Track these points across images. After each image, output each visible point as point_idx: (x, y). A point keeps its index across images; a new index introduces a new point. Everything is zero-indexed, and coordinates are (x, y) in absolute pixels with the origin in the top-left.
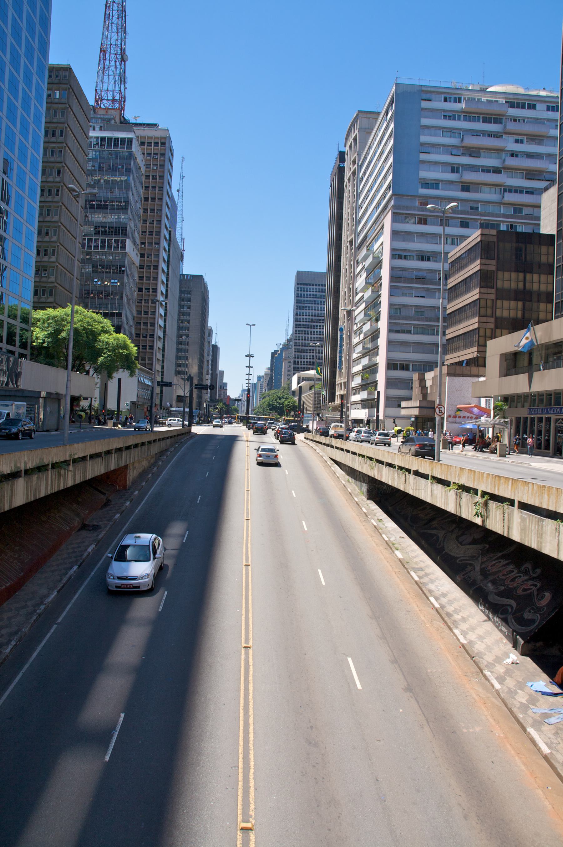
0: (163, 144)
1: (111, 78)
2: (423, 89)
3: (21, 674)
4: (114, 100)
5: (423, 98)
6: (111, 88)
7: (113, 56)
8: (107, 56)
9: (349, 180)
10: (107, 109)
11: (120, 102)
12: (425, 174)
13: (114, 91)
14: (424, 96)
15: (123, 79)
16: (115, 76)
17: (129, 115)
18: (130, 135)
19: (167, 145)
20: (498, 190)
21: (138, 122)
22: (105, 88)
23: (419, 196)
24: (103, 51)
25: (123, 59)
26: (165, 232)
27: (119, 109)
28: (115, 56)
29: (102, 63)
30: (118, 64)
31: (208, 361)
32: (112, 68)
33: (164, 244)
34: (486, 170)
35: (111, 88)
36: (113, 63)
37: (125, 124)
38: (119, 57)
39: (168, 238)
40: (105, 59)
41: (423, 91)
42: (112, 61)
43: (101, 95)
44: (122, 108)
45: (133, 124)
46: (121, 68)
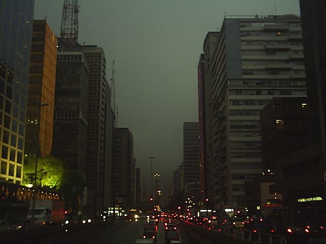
0: (100, 56)
1: (70, 22)
2: (240, 20)
3: (314, 199)
4: (71, 34)
5: (241, 25)
6: (70, 27)
7: (70, 10)
8: (68, 10)
9: (207, 69)
10: (67, 39)
11: (75, 35)
12: (247, 66)
13: (71, 29)
14: (242, 24)
15: (76, 22)
16: (72, 20)
17: (81, 41)
18: (81, 53)
19: (102, 57)
20: (235, 92)
21: (85, 45)
22: (66, 28)
23: (243, 79)
24: (65, 7)
25: (77, 11)
26: (101, 105)
27: (74, 38)
28: (72, 10)
29: (64, 14)
30: (73, 14)
31: (134, 179)
32: (70, 17)
33: (101, 112)
34: (280, 61)
35: (70, 27)
36: (70, 14)
37: (78, 45)
38: (74, 10)
39: (104, 109)
40: (66, 12)
41: (241, 22)
42: (70, 14)
43: (64, 31)
44: (76, 38)
45: (82, 46)
46: (75, 17)
